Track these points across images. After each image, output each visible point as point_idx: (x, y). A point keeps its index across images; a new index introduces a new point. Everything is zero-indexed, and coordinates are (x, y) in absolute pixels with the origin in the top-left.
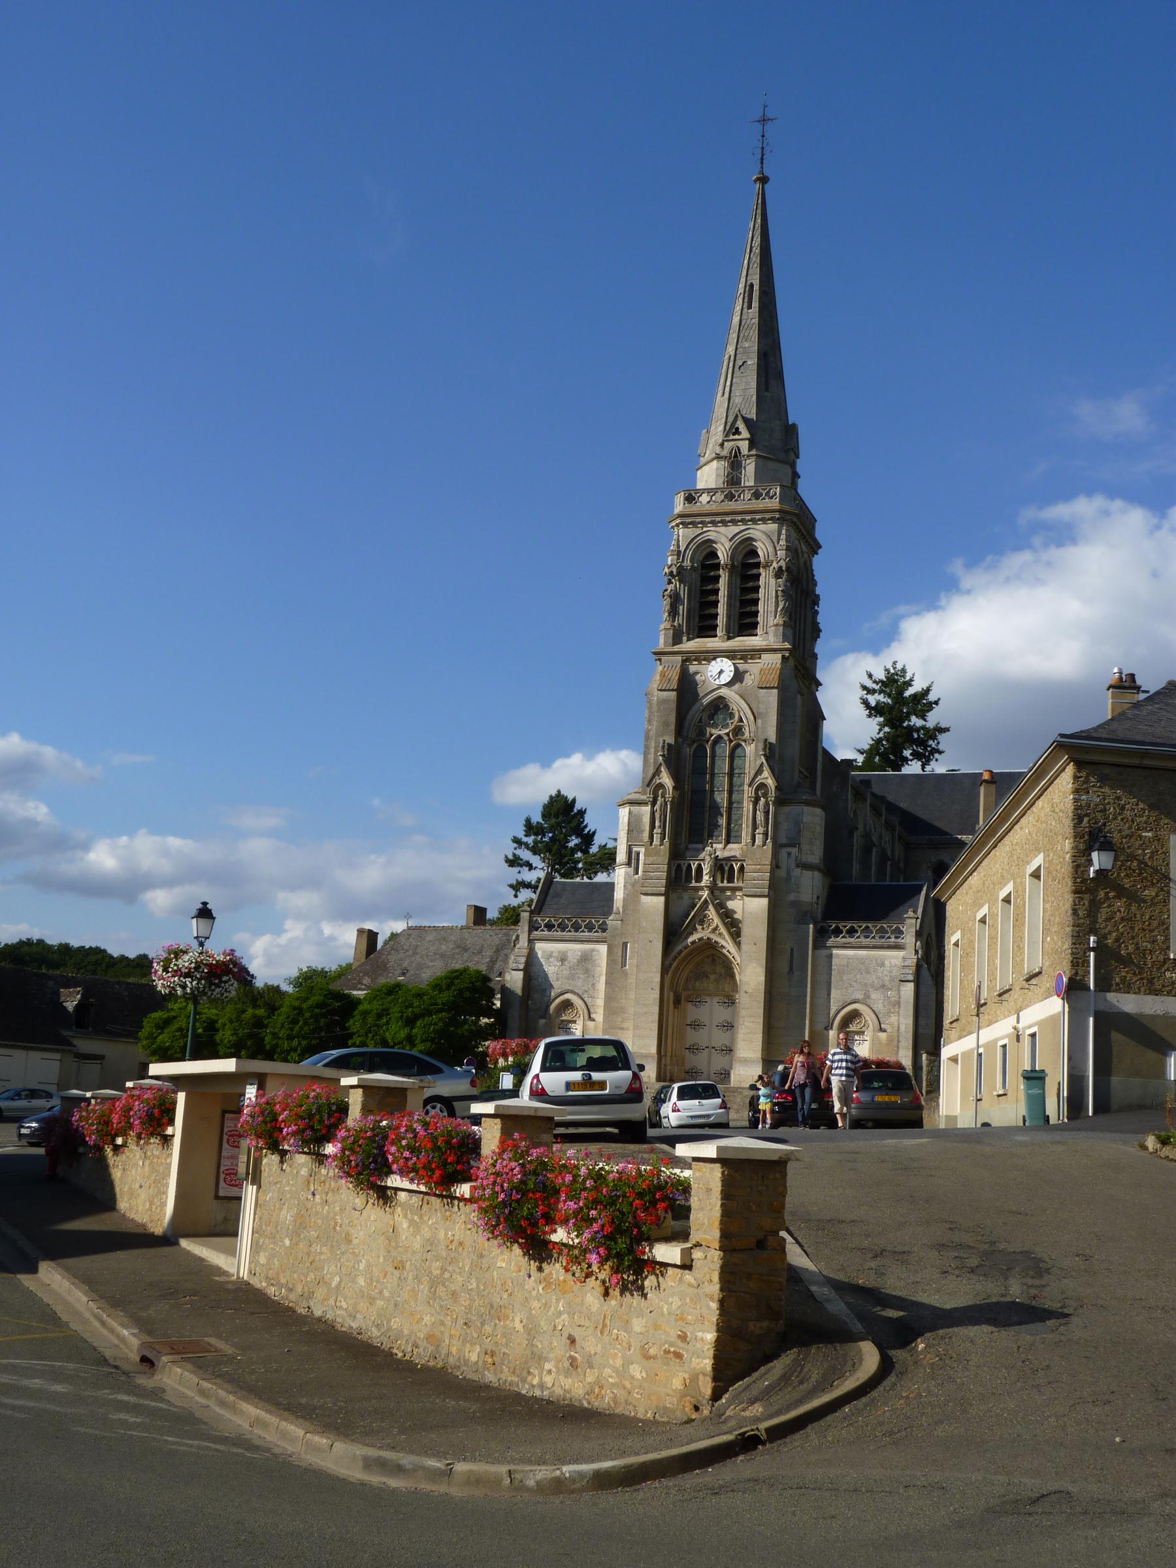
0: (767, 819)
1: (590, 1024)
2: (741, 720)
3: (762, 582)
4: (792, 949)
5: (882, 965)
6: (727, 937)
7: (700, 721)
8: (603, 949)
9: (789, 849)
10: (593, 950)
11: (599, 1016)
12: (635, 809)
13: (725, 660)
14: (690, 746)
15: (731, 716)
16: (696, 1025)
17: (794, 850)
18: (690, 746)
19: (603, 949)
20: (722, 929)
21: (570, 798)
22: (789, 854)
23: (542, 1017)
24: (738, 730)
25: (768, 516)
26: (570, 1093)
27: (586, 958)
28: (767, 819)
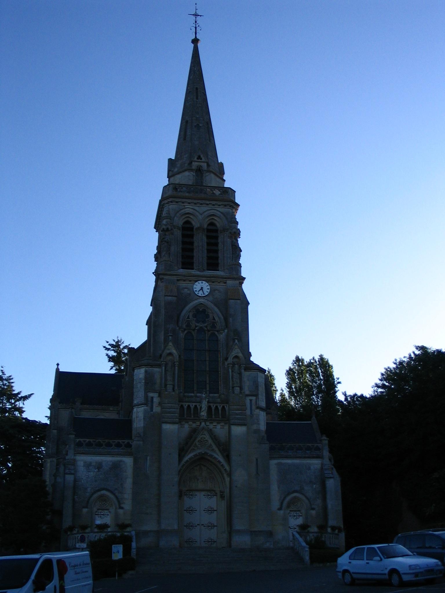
0: (174, 380)
1: (121, 511)
2: (214, 319)
3: (220, 240)
4: (257, 460)
5: (309, 469)
6: (217, 451)
7: (188, 318)
8: (129, 461)
9: (250, 398)
10: (121, 461)
11: (128, 505)
12: (150, 369)
13: (204, 282)
14: (183, 332)
15: (208, 316)
16: (190, 510)
17: (254, 398)
18: (183, 332)
19: (129, 461)
20: (214, 447)
21: (317, 358)
22: (251, 400)
23: (84, 507)
24: (214, 326)
25: (226, 203)
26: (417, 578)
27: (116, 467)
28: (174, 380)
